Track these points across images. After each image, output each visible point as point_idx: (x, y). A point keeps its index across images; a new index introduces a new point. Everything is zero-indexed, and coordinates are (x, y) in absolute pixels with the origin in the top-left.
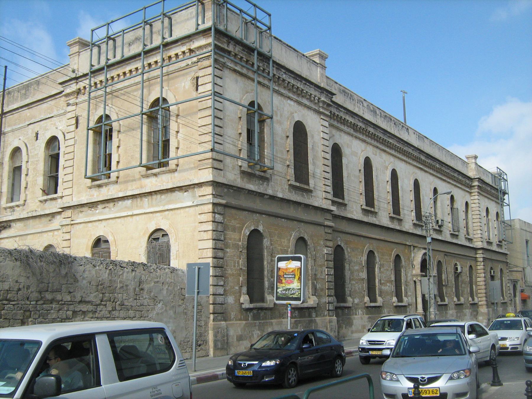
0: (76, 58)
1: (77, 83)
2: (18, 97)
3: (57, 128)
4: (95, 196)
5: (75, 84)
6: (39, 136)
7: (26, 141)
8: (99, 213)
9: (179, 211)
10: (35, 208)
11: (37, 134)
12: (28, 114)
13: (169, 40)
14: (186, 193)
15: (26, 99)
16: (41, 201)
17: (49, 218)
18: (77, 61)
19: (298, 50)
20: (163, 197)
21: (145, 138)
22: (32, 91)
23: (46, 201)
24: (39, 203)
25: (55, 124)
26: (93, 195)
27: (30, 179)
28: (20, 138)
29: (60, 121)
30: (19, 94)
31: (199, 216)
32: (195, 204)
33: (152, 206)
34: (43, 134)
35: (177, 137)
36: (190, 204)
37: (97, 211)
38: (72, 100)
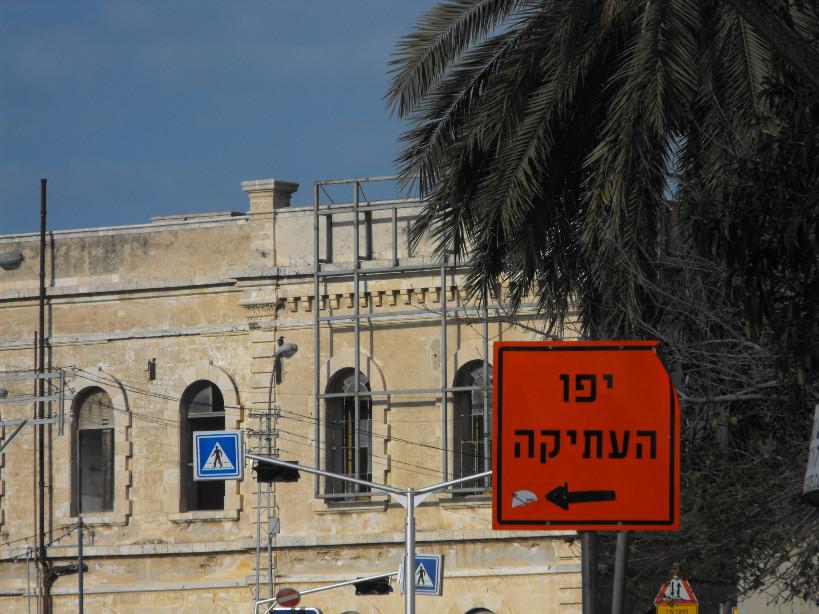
0: (269, 225)
1: (278, 285)
2: (81, 261)
3: (211, 363)
4: (333, 532)
5: (274, 287)
6: (158, 371)
7: (119, 376)
8: (342, 566)
9: (521, 580)
10: (157, 534)
11: (152, 367)
12: (121, 313)
13: (405, 263)
14: (534, 549)
15: (108, 271)
16: (174, 522)
17: (201, 560)
18: (271, 232)
19: (228, 378)
20: (488, 550)
21: (322, 437)
22: (126, 255)
23: (189, 522)
24: (170, 525)
25: (204, 353)
26: (329, 530)
27: (138, 465)
28: (101, 365)
29: (218, 349)
30: (86, 254)
31: (560, 594)
32: (553, 570)
33: (466, 565)
34: (171, 368)
35: (389, 459)
36: (544, 569)
37: (339, 563)
38: (264, 320)
